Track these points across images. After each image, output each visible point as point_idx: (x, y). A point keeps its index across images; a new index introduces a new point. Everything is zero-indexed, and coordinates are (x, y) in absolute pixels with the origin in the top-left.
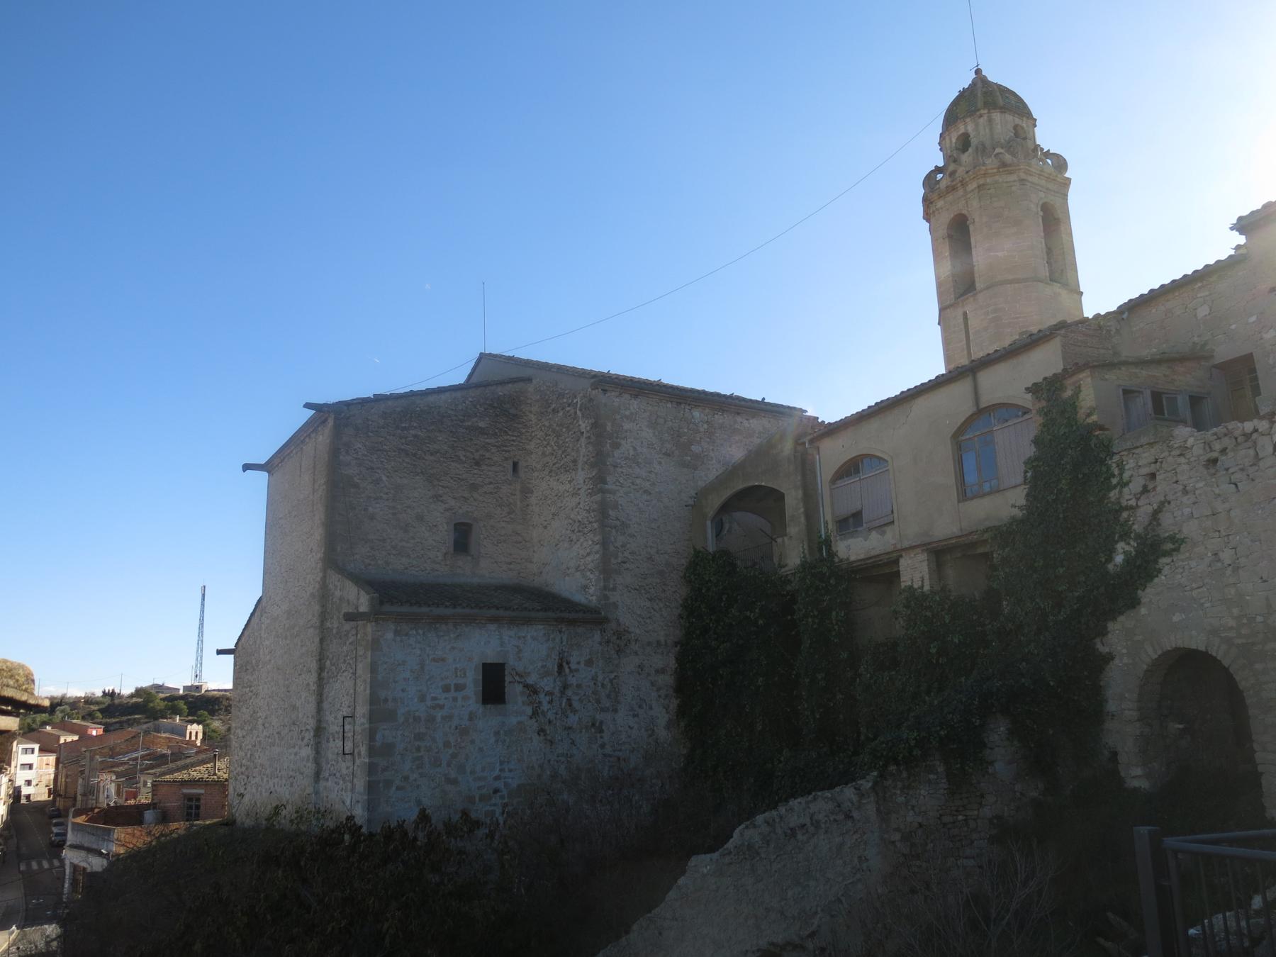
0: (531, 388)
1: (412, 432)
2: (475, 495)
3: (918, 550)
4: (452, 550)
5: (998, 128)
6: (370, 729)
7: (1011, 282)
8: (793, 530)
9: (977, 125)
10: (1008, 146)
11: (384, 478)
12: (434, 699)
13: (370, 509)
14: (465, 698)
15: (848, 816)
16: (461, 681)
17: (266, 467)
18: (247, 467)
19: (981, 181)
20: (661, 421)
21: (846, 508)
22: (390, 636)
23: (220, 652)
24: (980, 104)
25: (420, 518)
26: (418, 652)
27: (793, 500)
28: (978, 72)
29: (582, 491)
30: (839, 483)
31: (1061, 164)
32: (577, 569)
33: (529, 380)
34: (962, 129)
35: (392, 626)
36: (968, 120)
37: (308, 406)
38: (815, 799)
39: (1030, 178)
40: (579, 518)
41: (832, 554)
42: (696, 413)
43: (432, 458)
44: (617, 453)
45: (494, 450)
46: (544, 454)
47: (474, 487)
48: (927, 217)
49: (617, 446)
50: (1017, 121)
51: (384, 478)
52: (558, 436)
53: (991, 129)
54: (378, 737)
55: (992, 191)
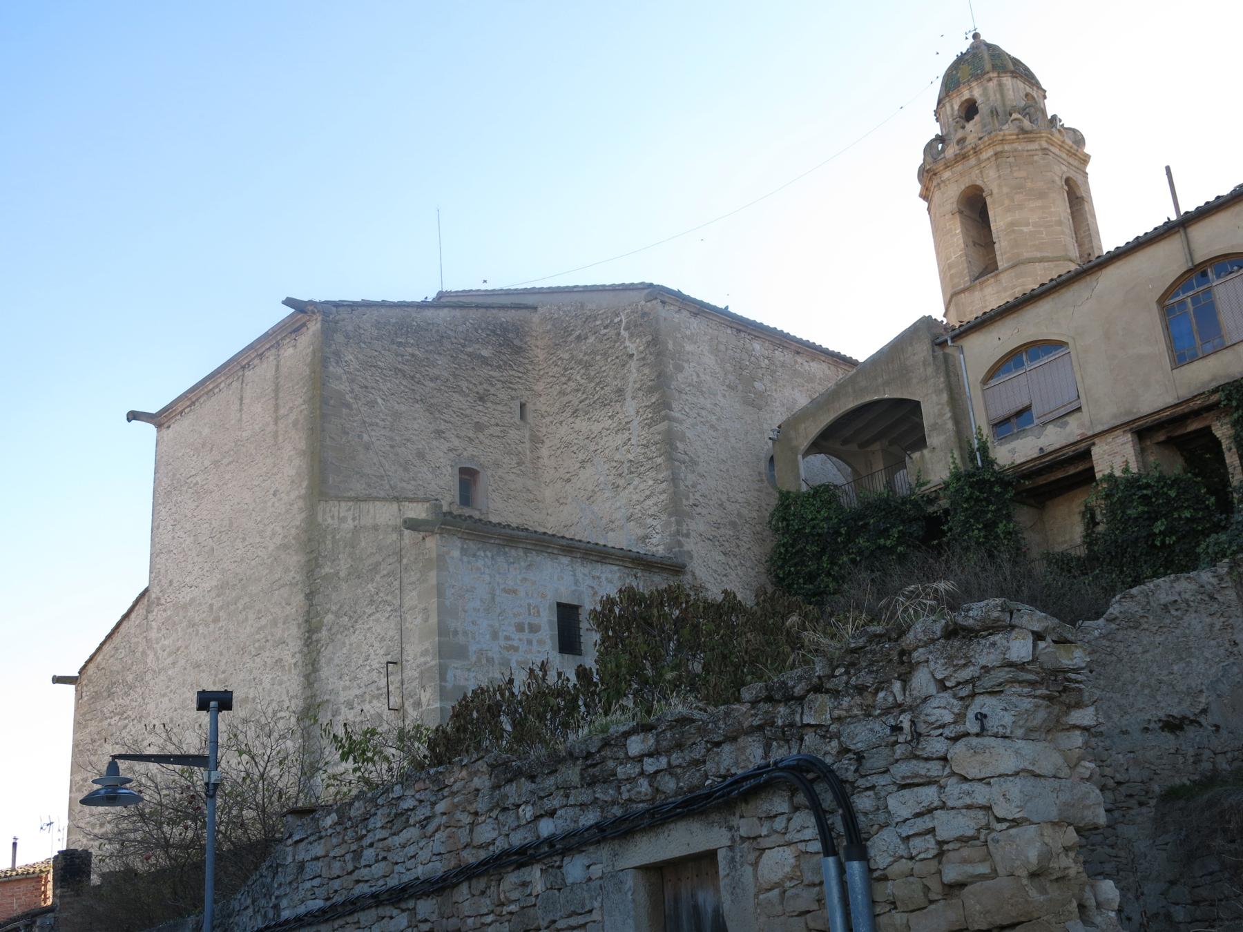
0: (536, 318)
1: (410, 350)
2: (481, 436)
3: (1119, 432)
4: (457, 500)
5: (1010, 94)
6: (440, 665)
7: (1041, 260)
8: (934, 440)
9: (985, 90)
10: (1024, 111)
11: (380, 401)
12: (507, 638)
13: (366, 437)
14: (541, 642)
15: (1212, 598)
16: (535, 621)
17: (160, 419)
18: (133, 416)
19: (999, 148)
20: (722, 348)
21: (1005, 408)
22: (456, 553)
23: (58, 680)
24: (988, 67)
25: (421, 455)
26: (487, 578)
27: (934, 410)
28: (976, 36)
29: (635, 423)
30: (992, 382)
31: (1079, 140)
32: (629, 519)
33: (535, 308)
34: (966, 95)
35: (458, 543)
36: (974, 84)
37: (289, 302)
38: (1178, 579)
39: (1052, 148)
40: (631, 457)
41: (989, 462)
42: (757, 346)
43: (432, 385)
44: (680, 377)
45: (499, 385)
46: (562, 393)
47: (479, 427)
48: (925, 195)
49: (680, 369)
50: (1028, 90)
51: (380, 401)
52: (587, 366)
53: (1002, 95)
54: (449, 676)
55: (1011, 160)
